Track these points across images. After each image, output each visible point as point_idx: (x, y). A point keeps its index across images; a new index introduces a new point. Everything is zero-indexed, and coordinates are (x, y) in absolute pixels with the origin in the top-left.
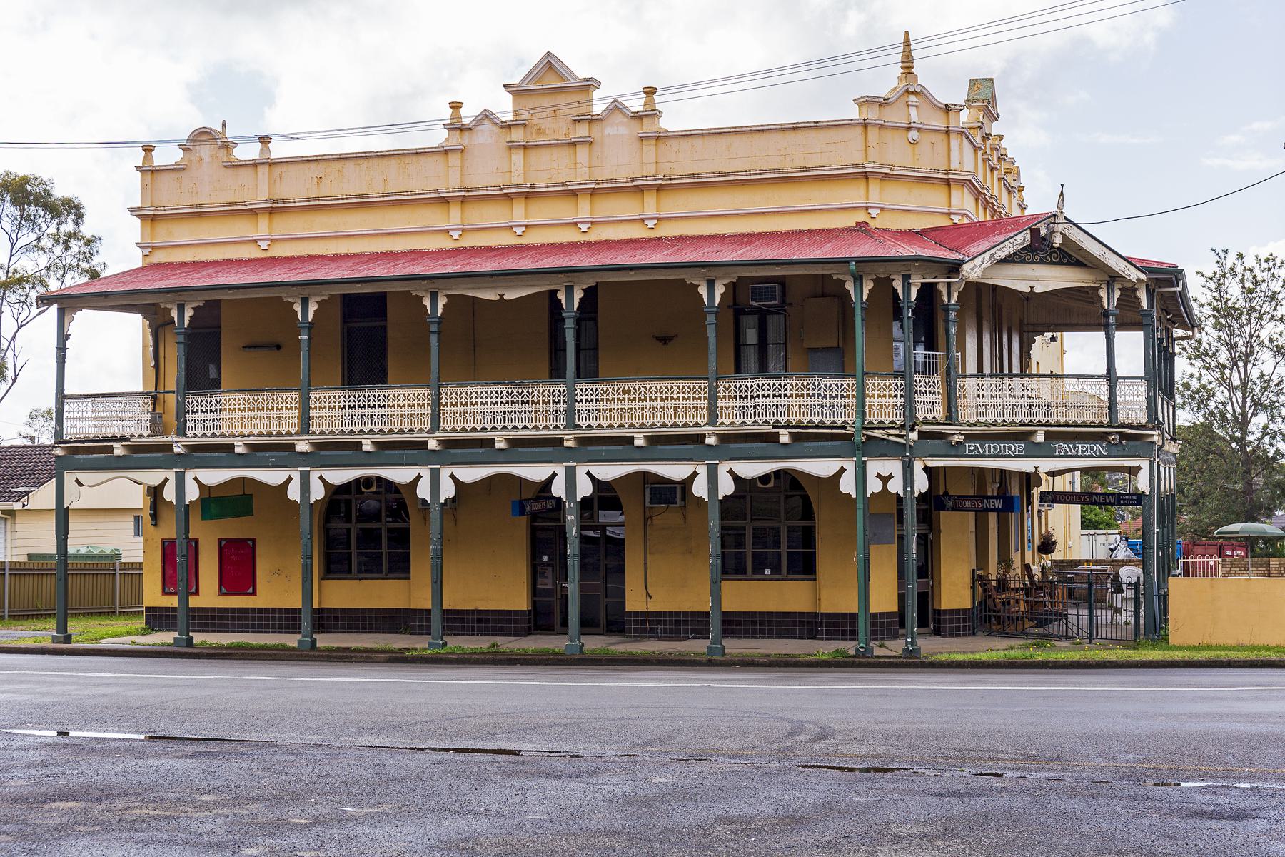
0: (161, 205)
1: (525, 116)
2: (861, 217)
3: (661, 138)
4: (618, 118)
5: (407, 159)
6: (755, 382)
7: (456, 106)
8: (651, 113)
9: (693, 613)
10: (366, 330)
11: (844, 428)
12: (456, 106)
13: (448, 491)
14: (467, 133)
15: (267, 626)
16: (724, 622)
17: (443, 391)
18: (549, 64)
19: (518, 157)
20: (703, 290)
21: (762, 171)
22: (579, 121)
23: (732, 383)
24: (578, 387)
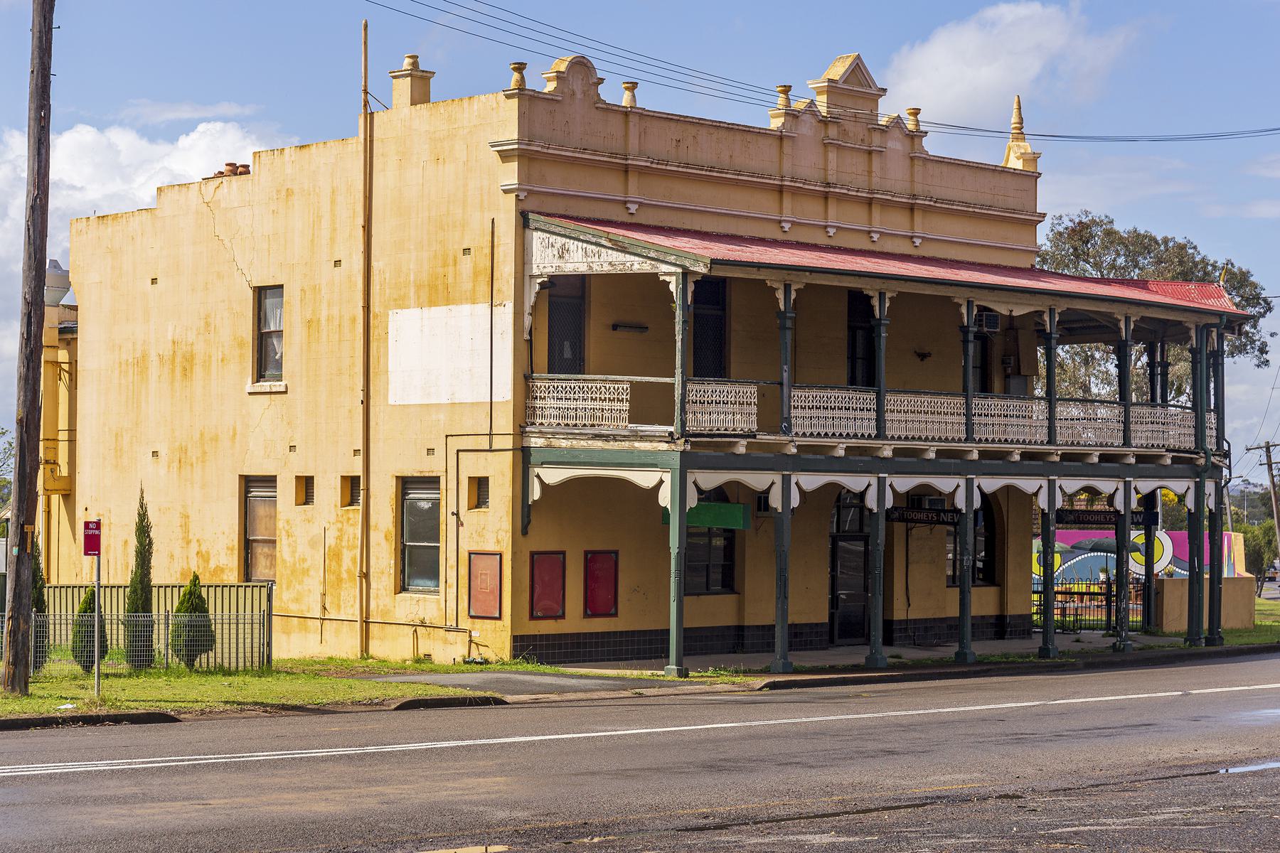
5: (749, 137)
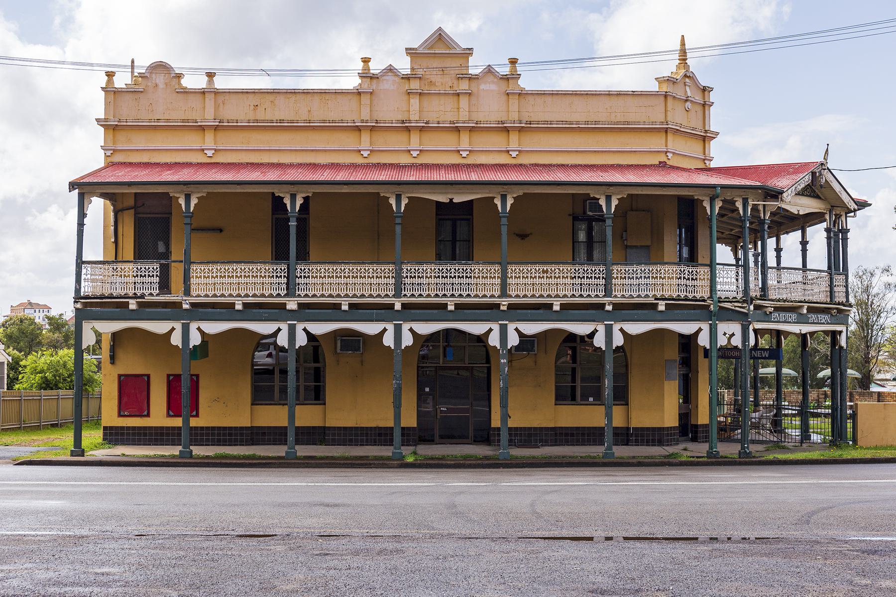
0: (123, 118)
1: (420, 72)
2: (663, 158)
3: (522, 94)
4: (491, 78)
5: (327, 97)
6: (639, 267)
7: (366, 61)
8: (513, 77)
9: (541, 429)
10: (289, 223)
11: (704, 301)
12: (366, 61)
13: (513, 340)
14: (375, 81)
15: (208, 440)
16: (403, 435)
17: (404, 267)
18: (440, 37)
19: (415, 101)
20: (393, 201)
21: (596, 122)
22: (462, 78)
23: (623, 268)
24: (298, 267)
